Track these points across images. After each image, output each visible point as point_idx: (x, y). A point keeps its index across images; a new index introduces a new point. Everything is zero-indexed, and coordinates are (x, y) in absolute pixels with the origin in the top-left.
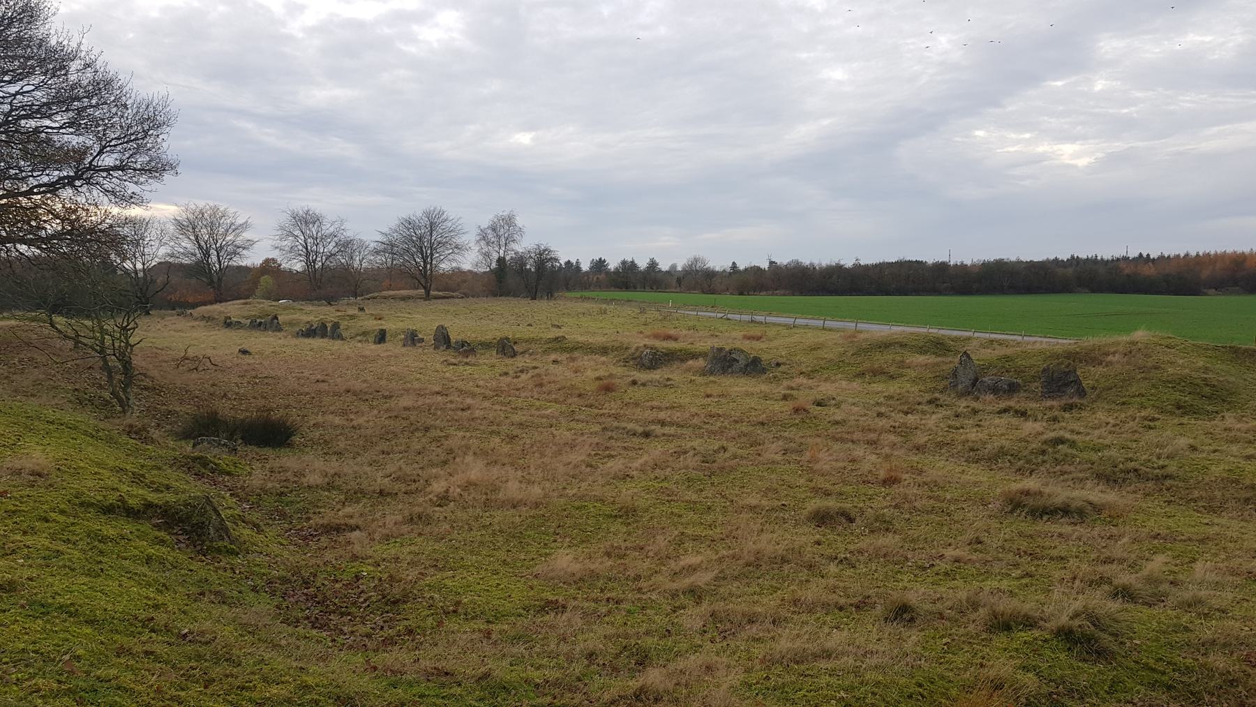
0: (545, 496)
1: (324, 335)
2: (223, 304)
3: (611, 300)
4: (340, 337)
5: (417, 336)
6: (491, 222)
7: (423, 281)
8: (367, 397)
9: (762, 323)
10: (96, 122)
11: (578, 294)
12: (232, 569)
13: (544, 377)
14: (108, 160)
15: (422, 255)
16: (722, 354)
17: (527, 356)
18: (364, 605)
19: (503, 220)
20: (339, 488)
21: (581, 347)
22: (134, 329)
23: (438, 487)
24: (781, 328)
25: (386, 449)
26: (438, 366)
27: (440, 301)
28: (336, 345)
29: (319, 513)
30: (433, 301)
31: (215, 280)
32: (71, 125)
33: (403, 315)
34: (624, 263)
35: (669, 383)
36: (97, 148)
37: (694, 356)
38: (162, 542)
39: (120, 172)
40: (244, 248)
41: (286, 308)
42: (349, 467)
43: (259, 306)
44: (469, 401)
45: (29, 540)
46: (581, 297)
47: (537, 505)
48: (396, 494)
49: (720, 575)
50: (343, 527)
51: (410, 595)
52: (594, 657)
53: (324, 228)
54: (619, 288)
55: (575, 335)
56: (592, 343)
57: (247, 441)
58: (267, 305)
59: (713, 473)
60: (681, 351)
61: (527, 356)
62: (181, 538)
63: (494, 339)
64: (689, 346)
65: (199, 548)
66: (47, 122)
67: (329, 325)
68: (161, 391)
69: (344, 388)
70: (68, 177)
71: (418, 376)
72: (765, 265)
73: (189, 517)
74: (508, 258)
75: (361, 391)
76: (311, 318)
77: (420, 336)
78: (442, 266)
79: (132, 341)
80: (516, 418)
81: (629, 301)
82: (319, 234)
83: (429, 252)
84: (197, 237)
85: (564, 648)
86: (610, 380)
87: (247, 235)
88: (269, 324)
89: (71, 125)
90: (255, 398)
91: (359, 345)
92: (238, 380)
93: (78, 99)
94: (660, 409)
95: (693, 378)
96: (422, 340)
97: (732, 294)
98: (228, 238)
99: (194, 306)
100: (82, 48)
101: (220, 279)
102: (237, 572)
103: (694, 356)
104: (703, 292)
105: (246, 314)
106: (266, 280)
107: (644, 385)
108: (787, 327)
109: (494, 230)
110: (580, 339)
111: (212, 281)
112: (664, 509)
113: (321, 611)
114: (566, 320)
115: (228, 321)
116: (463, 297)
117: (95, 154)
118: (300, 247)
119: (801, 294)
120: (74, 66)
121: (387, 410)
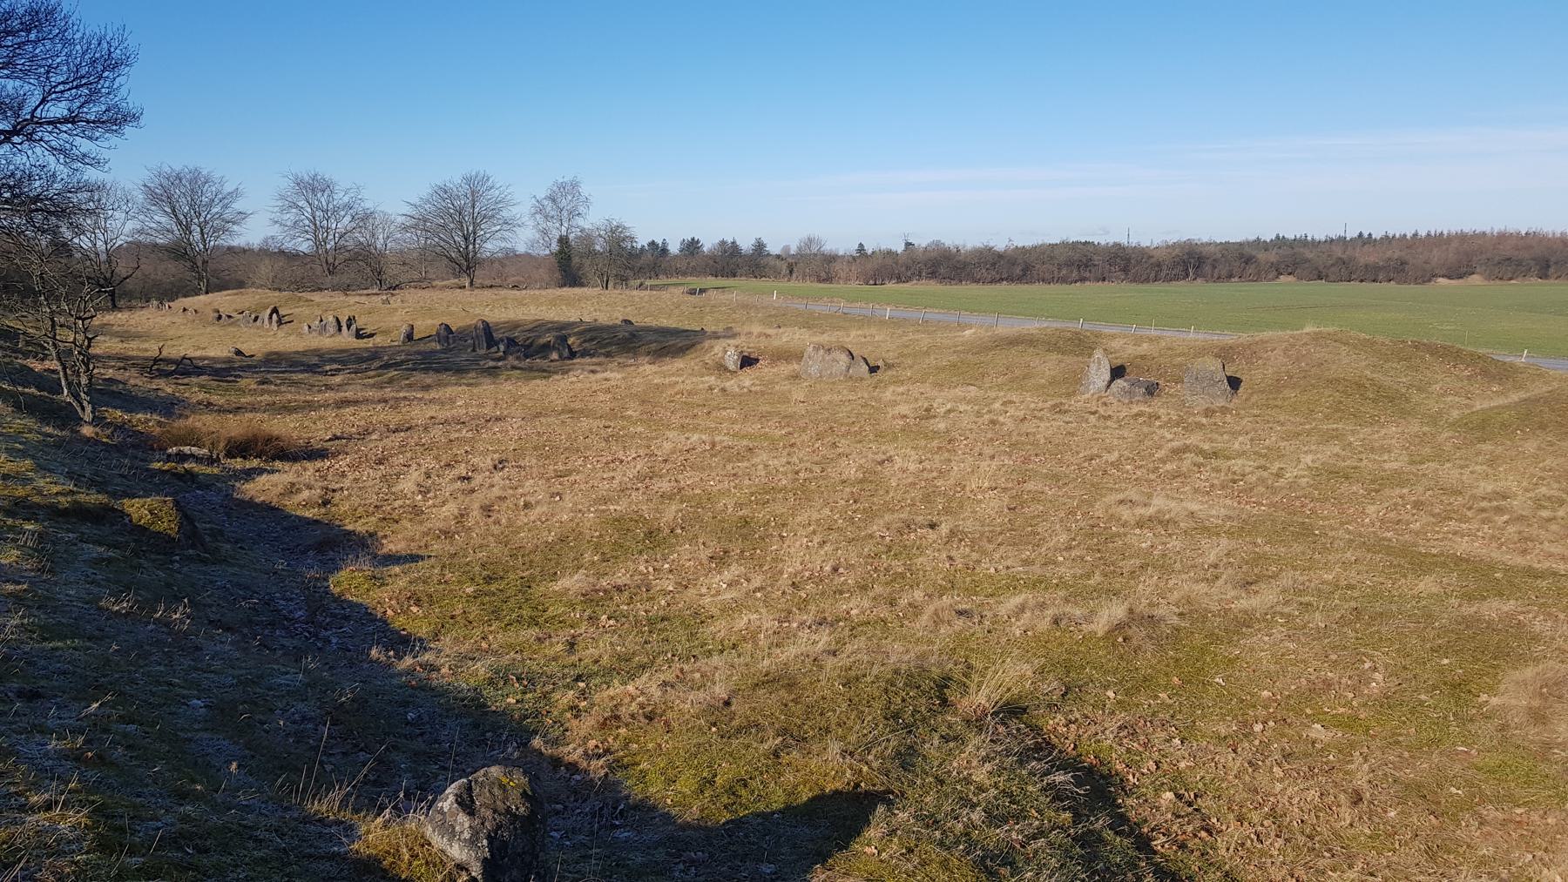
14: (57, 110)
39: (70, 125)
40: (234, 223)
72: (899, 248)
74: (571, 237)
78: (488, 246)
82: (331, 206)
84: (174, 211)
98: (214, 210)
118: (307, 222)
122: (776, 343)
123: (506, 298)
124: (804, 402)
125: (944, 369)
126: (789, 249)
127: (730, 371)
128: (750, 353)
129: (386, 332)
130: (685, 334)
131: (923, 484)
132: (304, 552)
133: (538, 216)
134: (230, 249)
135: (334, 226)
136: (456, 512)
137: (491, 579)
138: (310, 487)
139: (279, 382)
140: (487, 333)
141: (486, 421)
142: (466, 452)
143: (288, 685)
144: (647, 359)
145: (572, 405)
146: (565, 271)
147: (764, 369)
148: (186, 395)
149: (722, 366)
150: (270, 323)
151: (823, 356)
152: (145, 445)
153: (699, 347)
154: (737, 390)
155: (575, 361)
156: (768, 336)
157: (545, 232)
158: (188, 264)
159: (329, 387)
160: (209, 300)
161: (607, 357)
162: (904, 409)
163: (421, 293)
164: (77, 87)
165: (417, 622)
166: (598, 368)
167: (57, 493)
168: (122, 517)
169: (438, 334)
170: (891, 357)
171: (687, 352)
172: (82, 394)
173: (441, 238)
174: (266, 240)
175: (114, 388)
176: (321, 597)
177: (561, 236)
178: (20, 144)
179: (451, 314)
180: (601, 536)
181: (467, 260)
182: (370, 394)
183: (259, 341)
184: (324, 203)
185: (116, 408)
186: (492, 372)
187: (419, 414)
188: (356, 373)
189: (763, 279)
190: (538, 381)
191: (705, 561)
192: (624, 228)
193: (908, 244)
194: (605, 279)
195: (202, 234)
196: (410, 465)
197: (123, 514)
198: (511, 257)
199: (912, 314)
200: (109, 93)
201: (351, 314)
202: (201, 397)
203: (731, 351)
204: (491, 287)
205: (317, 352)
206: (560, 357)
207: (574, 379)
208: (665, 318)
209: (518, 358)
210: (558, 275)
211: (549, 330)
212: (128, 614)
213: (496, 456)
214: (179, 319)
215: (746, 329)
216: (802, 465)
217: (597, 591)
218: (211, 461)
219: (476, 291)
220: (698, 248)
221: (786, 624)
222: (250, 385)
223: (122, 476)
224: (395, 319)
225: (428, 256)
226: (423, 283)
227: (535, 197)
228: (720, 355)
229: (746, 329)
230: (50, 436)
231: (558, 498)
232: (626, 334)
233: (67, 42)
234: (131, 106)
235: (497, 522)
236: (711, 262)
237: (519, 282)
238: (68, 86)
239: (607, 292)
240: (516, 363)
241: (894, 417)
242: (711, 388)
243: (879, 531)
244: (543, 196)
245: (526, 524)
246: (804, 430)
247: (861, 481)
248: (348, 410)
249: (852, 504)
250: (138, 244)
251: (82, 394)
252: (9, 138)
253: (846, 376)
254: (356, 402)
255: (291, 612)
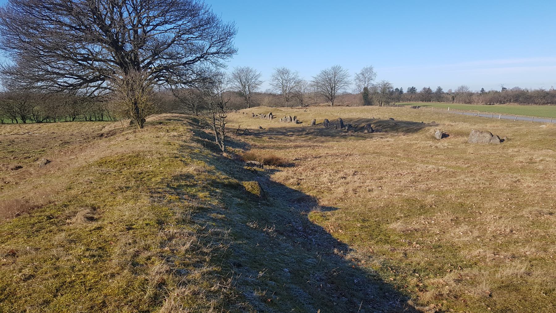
39: (217, 55)
40: (258, 85)
72: (499, 90)
74: (369, 87)
82: (288, 79)
84: (241, 81)
98: (253, 81)
118: (280, 84)
122: (456, 129)
123: (345, 110)
124: (472, 153)
125: (535, 142)
126: (451, 91)
127: (437, 139)
128: (445, 132)
129: (306, 122)
130: (417, 124)
131: (540, 193)
132: (294, 202)
133: (357, 80)
134: (255, 93)
135: (289, 85)
136: (344, 191)
137: (364, 220)
138: (293, 178)
139: (275, 138)
140: (341, 123)
141: (346, 155)
142: (342, 167)
143: (312, 263)
144: (402, 133)
145: (376, 151)
146: (366, 100)
147: (452, 139)
148: (248, 142)
149: (434, 137)
150: (269, 118)
151: (479, 135)
152: (240, 160)
153: (423, 129)
154: (442, 147)
155: (374, 133)
156: (452, 126)
157: (359, 86)
158: (244, 98)
159: (291, 141)
160: (251, 110)
161: (386, 132)
162: (521, 159)
163: (316, 108)
164: (220, 42)
165: (342, 236)
166: (383, 136)
167: (223, 179)
168: (242, 188)
169: (324, 123)
170: (509, 136)
171: (418, 131)
172: (222, 142)
173: (322, 89)
174: (267, 90)
175: (228, 139)
176: (306, 222)
177: (365, 87)
178: (203, 61)
179: (327, 115)
180: (402, 206)
181: (331, 96)
182: (302, 144)
183: (267, 124)
184: (286, 78)
185: (230, 146)
186: (345, 137)
187: (322, 152)
188: (298, 136)
189: (442, 102)
190: (361, 141)
191: (450, 221)
192: (389, 84)
193: (504, 89)
194: (381, 103)
195: (249, 89)
196: (323, 171)
197: (243, 187)
198: (346, 95)
199: (509, 117)
200: (228, 44)
201: (295, 115)
202: (252, 143)
203: (438, 132)
204: (339, 105)
205: (284, 128)
206: (368, 132)
207: (375, 140)
208: (405, 117)
209: (352, 132)
210: (363, 101)
211: (363, 122)
212: (256, 228)
213: (354, 170)
214: (242, 116)
215: (442, 123)
216: (480, 181)
217: (408, 230)
218: (260, 166)
219: (334, 107)
220: (415, 90)
221: (497, 256)
222: (266, 139)
223: (238, 171)
224: (309, 117)
225: (317, 95)
226: (316, 104)
228: (432, 133)
229: (442, 123)
230: (215, 156)
231: (380, 188)
232: (393, 124)
233: (218, 28)
234: (235, 48)
235: (359, 196)
236: (421, 96)
237: (348, 104)
238: (217, 42)
239: (381, 107)
240: (352, 134)
241: (516, 162)
242: (431, 146)
243: (526, 214)
244: (359, 73)
245: (370, 198)
246: (475, 165)
247: (511, 190)
248: (299, 149)
249: (509, 201)
250: (230, 92)
251: (222, 142)
253: (489, 143)
254: (300, 147)
255: (297, 227)
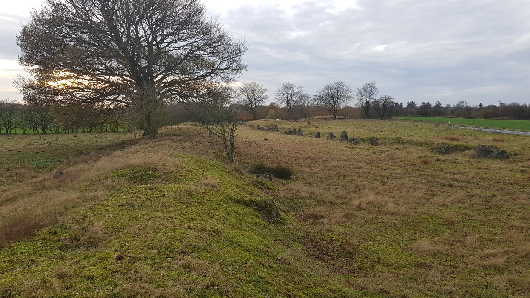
0: (407, 211)
1: (295, 134)
2: (257, 120)
3: (420, 121)
4: (301, 135)
5: (333, 135)
6: (363, 87)
7: (333, 112)
8: (317, 160)
9: (500, 133)
10: (220, 51)
11: (403, 118)
12: (283, 230)
13: (393, 156)
14: (223, 66)
15: (333, 101)
16: (484, 148)
17: (383, 145)
18: (337, 253)
19: (369, 85)
20: (313, 199)
21: (409, 142)
22: (235, 130)
23: (356, 202)
24: (510, 136)
25: (329, 184)
26: (344, 148)
27: (341, 120)
28: (300, 138)
29: (307, 209)
30: (337, 120)
31: (254, 111)
32: (211, 53)
33: (326, 126)
34: (424, 103)
35: (456, 161)
36: (219, 61)
37: (469, 148)
38: (257, 217)
39: (227, 70)
40: (264, 99)
41: (280, 123)
42: (316, 190)
43: (270, 122)
44: (360, 164)
45: (217, 213)
46: (404, 119)
47: (403, 215)
48: (338, 204)
49: (508, 260)
50: (318, 216)
51: (356, 251)
52: (452, 294)
53: (294, 90)
54: (422, 115)
55: (406, 137)
56: (414, 141)
57: (275, 176)
58: (272, 121)
59: (491, 208)
60: (461, 146)
61: (383, 145)
62: (263, 215)
63: (367, 137)
64: (465, 144)
65: (270, 220)
66: (203, 52)
67: (297, 130)
68: (241, 154)
69: (307, 156)
70: (209, 73)
71: (336, 152)
72: (498, 105)
73: (266, 207)
74: (370, 102)
75: (314, 158)
76: (290, 127)
77: (334, 135)
78: (342, 105)
79: (235, 135)
80: (384, 173)
81: (428, 121)
82: (293, 93)
83: (336, 99)
84: (248, 95)
85: (435, 287)
86: (425, 159)
87: (265, 94)
88: (273, 129)
89: (211, 53)
90: (273, 158)
91: (309, 138)
92: (266, 151)
93: (214, 43)
94: (454, 173)
95: (469, 159)
96: (335, 137)
97: (480, 118)
98: (259, 95)
99: (246, 121)
100: (216, 23)
101: (255, 111)
102: (285, 232)
103: (469, 148)
104: (465, 118)
105: (265, 124)
106: (271, 111)
107: (444, 161)
108: (514, 135)
109: (365, 89)
110: (408, 138)
111: (253, 112)
112: (468, 223)
113: (320, 253)
114: (398, 130)
115: (259, 127)
116: (349, 119)
117: (218, 64)
118: (285, 98)
119: (519, 119)
120: (214, 30)
121: (326, 167)
126: (450, 105)
164: (230, 59)
227: (358, 88)
252: (211, 74)
